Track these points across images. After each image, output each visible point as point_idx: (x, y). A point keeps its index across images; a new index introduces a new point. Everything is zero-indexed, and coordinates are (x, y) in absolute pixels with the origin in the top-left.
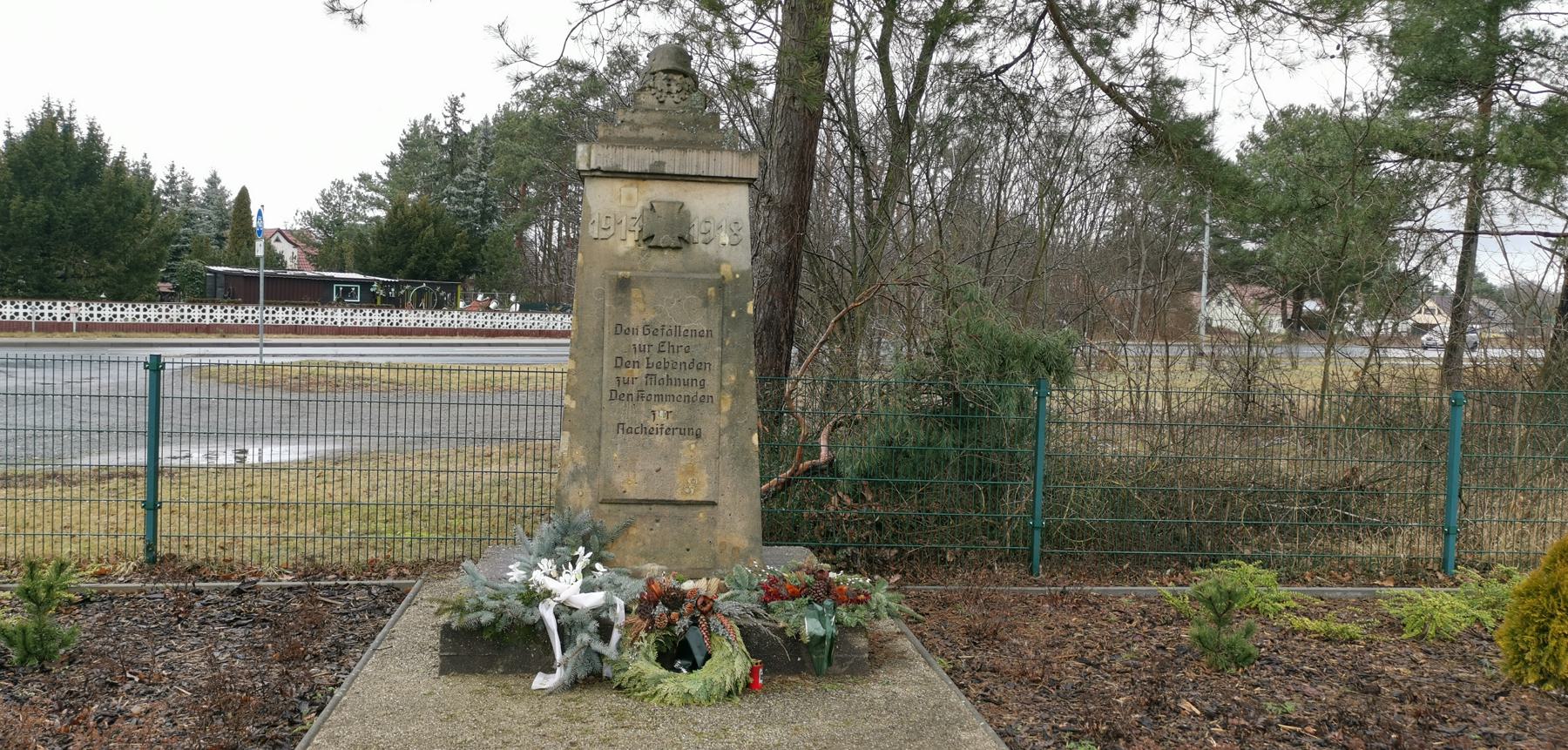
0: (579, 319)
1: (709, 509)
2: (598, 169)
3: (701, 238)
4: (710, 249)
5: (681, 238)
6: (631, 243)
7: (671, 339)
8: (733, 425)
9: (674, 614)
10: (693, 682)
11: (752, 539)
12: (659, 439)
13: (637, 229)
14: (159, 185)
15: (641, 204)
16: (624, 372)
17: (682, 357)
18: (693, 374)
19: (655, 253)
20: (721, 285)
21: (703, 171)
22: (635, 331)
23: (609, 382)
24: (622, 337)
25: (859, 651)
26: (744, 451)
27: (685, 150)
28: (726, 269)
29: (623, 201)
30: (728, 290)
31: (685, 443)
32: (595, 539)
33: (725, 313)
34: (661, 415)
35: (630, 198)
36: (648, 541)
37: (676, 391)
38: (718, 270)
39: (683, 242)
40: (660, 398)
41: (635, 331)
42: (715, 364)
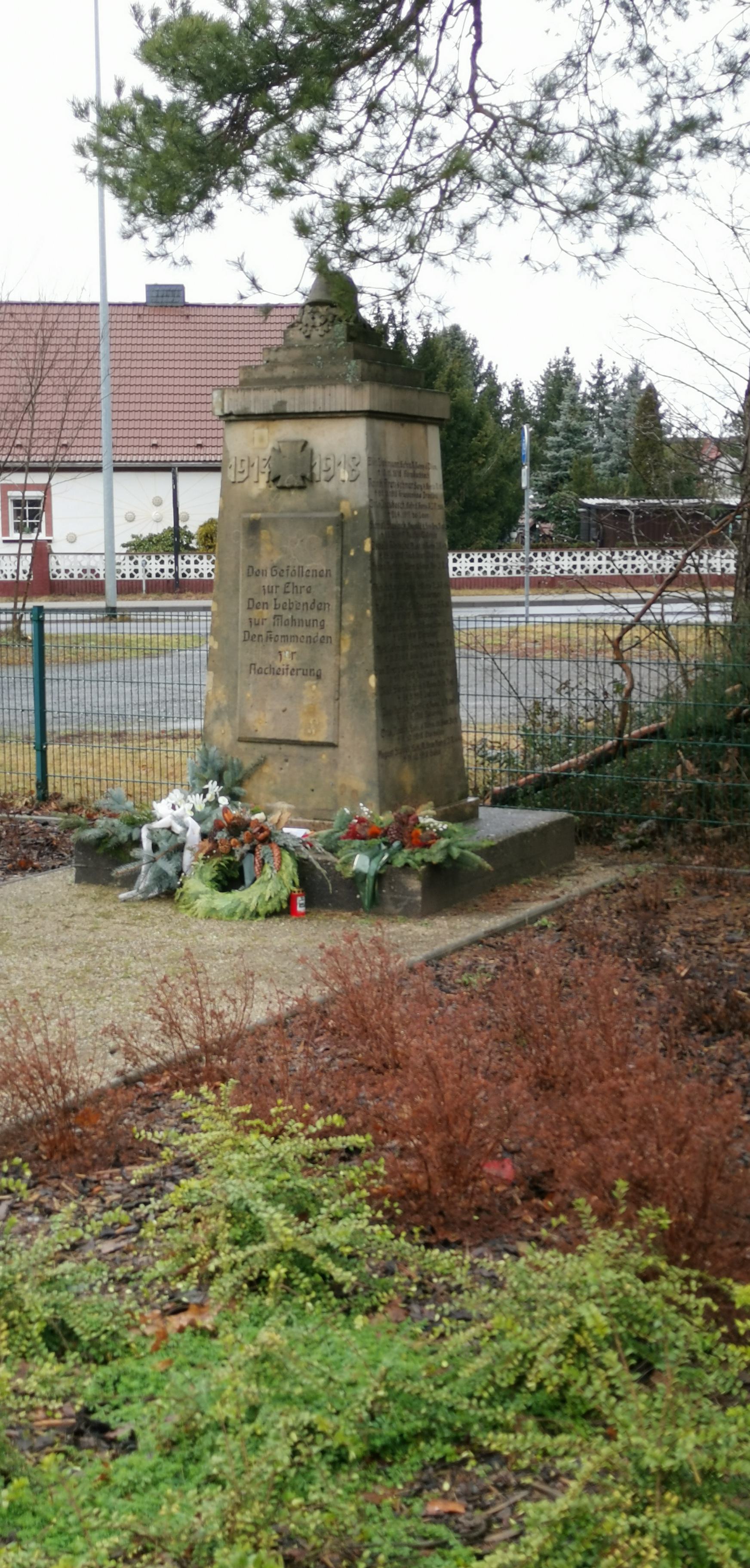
0: (220, 563)
1: (330, 750)
2: (230, 414)
3: (324, 476)
4: (331, 486)
5: (303, 478)
6: (263, 484)
7: (295, 580)
8: (352, 666)
9: (233, 841)
10: (224, 901)
11: (369, 782)
12: (286, 679)
13: (267, 470)
14: (585, 388)
15: (271, 446)
16: (255, 614)
17: (305, 598)
18: (313, 615)
19: (283, 494)
20: (340, 523)
21: (320, 408)
22: (263, 573)
23: (243, 626)
24: (253, 579)
25: (413, 894)
26: (362, 691)
27: (302, 387)
28: (345, 507)
29: (257, 444)
30: (348, 529)
31: (307, 684)
32: (227, 775)
33: (344, 551)
34: (287, 654)
35: (262, 440)
36: (279, 780)
37: (300, 631)
38: (338, 507)
39: (306, 481)
40: (286, 639)
41: (263, 573)
42: (334, 603)
